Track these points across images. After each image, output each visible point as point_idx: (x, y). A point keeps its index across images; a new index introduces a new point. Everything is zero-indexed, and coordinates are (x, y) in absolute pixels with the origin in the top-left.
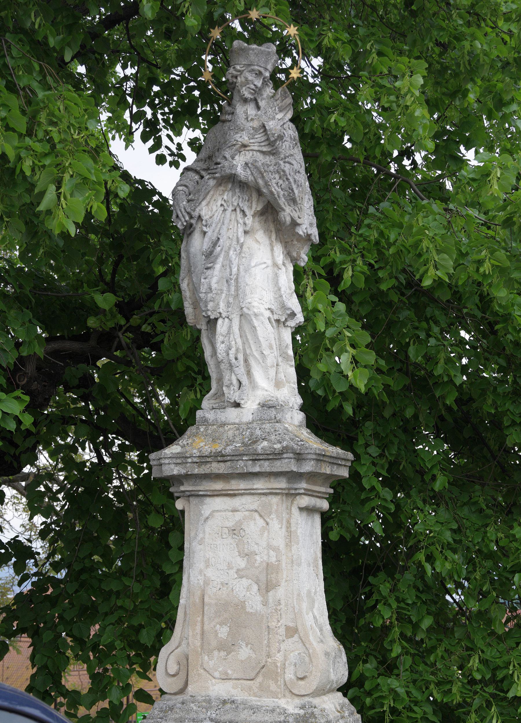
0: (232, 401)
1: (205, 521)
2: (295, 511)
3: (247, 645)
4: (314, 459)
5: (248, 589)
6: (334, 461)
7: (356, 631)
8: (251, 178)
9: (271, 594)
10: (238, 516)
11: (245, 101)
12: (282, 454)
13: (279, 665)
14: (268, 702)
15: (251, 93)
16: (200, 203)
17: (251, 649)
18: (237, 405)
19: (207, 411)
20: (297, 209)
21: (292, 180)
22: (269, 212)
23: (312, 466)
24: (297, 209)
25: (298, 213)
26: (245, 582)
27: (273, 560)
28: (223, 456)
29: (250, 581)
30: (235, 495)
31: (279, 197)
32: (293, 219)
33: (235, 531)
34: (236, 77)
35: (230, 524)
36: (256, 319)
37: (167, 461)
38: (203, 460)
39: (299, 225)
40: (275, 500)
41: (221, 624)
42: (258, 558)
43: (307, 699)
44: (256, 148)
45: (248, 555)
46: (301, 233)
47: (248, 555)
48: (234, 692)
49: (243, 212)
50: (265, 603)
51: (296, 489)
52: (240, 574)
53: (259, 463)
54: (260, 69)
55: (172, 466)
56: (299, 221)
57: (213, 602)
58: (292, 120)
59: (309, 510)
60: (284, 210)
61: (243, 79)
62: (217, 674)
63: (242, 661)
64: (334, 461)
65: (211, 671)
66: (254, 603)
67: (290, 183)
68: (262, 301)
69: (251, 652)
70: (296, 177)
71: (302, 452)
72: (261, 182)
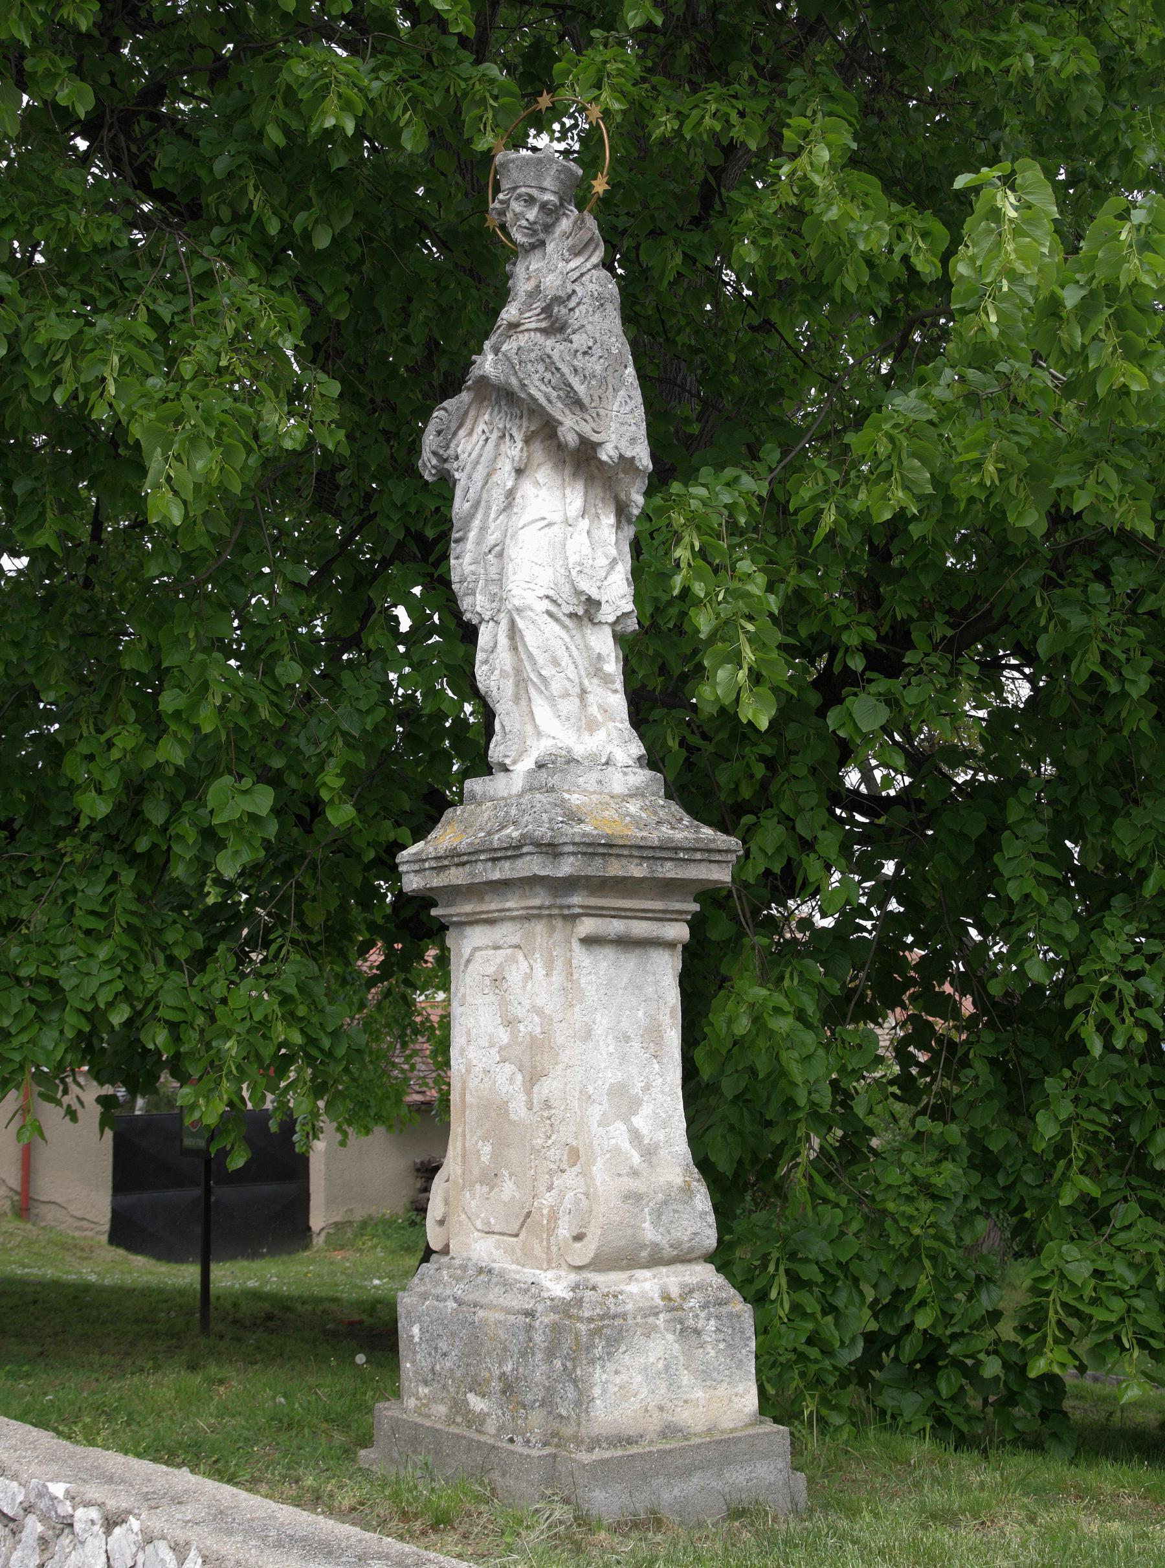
1: (466, 966)
2: (576, 945)
4: (573, 854)
5: (511, 1080)
6: (709, 853)
12: (521, 846)
13: (545, 1212)
14: (529, 1273)
15: (526, 235)
16: (455, 434)
20: (588, 418)
21: (565, 369)
23: (572, 865)
24: (588, 418)
25: (594, 425)
26: (508, 1068)
28: (459, 855)
31: (550, 402)
33: (498, 981)
35: (491, 970)
36: (522, 618)
39: (600, 444)
40: (539, 927)
41: (485, 1139)
42: (521, 1027)
43: (586, 1275)
44: (533, 325)
47: (510, 1022)
48: (497, 1254)
51: (569, 907)
54: (528, 190)
56: (595, 438)
57: (474, 1101)
60: (561, 423)
63: (505, 1204)
64: (709, 853)
67: (563, 375)
68: (532, 586)
70: (576, 363)
71: (556, 841)
72: (514, 381)
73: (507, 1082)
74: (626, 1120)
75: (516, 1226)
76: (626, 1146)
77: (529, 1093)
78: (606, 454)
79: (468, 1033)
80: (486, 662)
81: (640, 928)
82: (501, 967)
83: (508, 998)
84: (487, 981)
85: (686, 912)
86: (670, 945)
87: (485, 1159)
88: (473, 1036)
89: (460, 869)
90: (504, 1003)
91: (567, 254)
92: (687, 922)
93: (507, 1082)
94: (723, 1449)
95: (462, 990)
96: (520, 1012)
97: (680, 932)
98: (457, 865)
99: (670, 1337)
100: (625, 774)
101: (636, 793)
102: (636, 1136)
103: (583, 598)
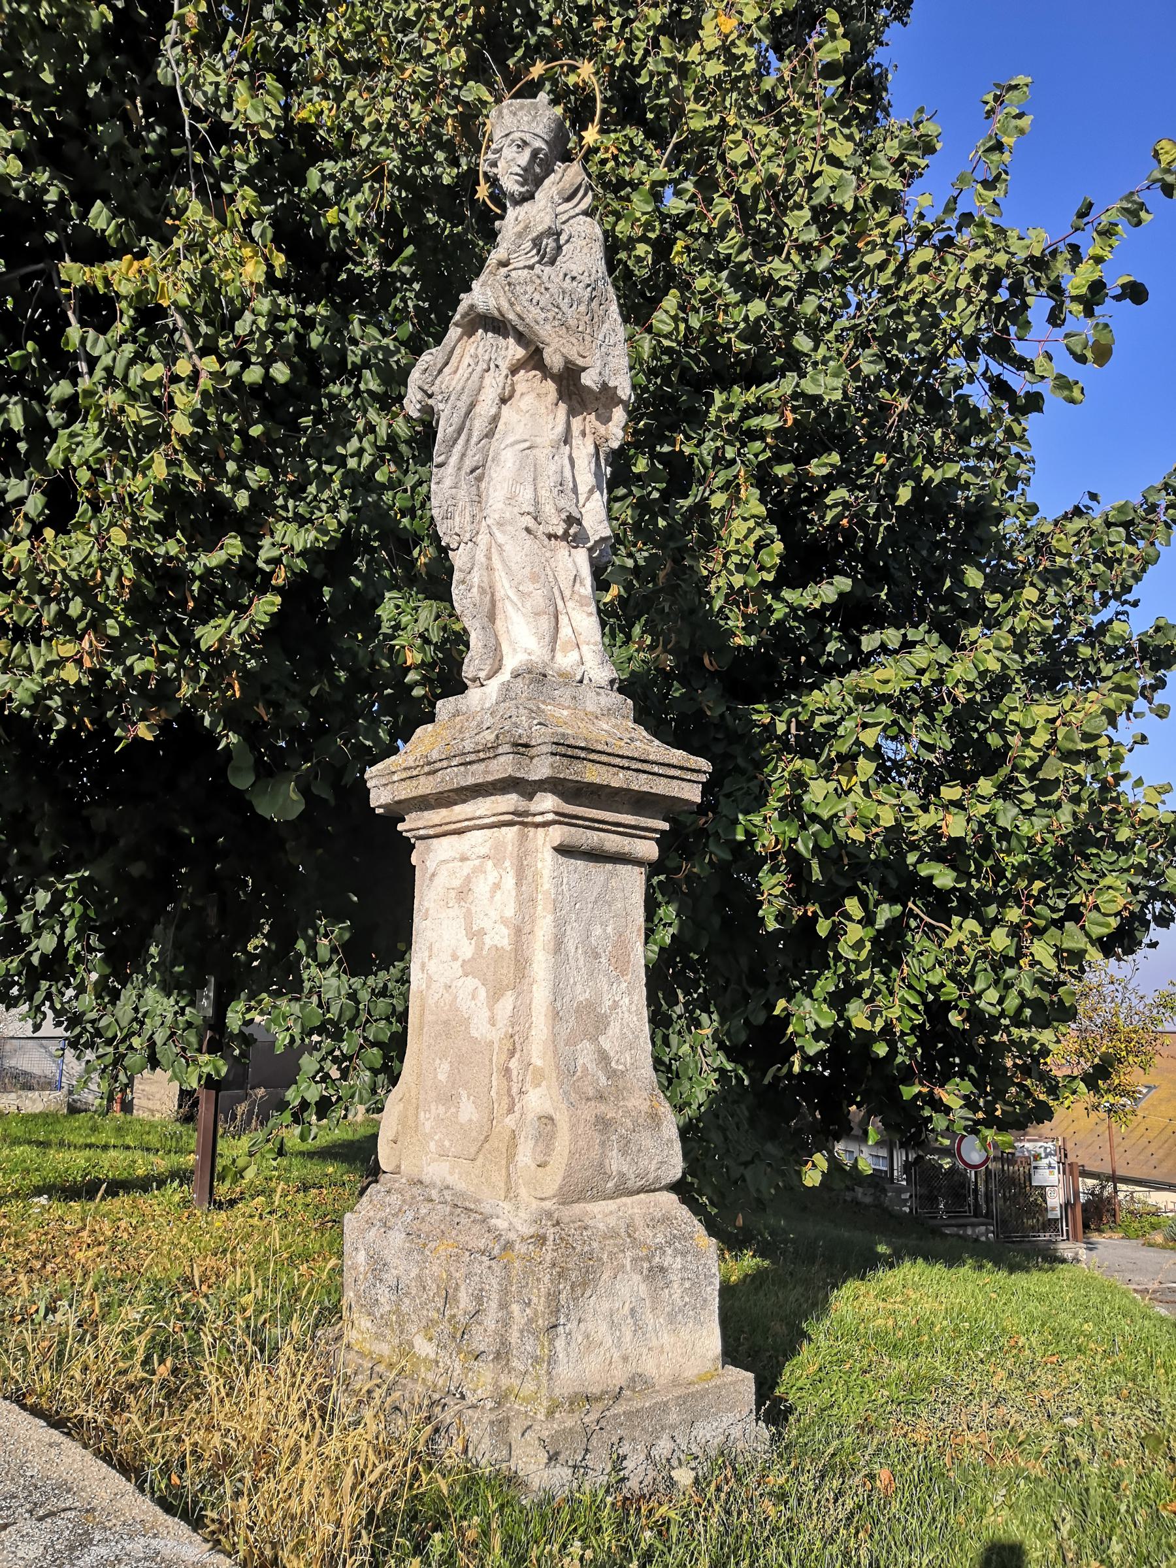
16: (440, 371)
35: (457, 883)
44: (521, 264)
56: (580, 362)
73: (471, 997)
74: (594, 1039)
75: (473, 1150)
76: (592, 1067)
77: (491, 1009)
78: (589, 379)
79: (430, 948)
80: (463, 582)
81: (613, 842)
82: (468, 879)
83: (473, 909)
84: (453, 894)
85: (655, 831)
86: (638, 862)
87: (442, 1077)
88: (435, 950)
89: (430, 778)
90: (468, 917)
91: (556, 198)
92: (657, 841)
93: (471, 997)
94: (694, 1402)
95: (426, 904)
96: (486, 924)
97: (649, 850)
98: (428, 774)
99: (637, 1278)
100: (598, 694)
101: (609, 712)
102: (603, 1058)
103: (564, 516)
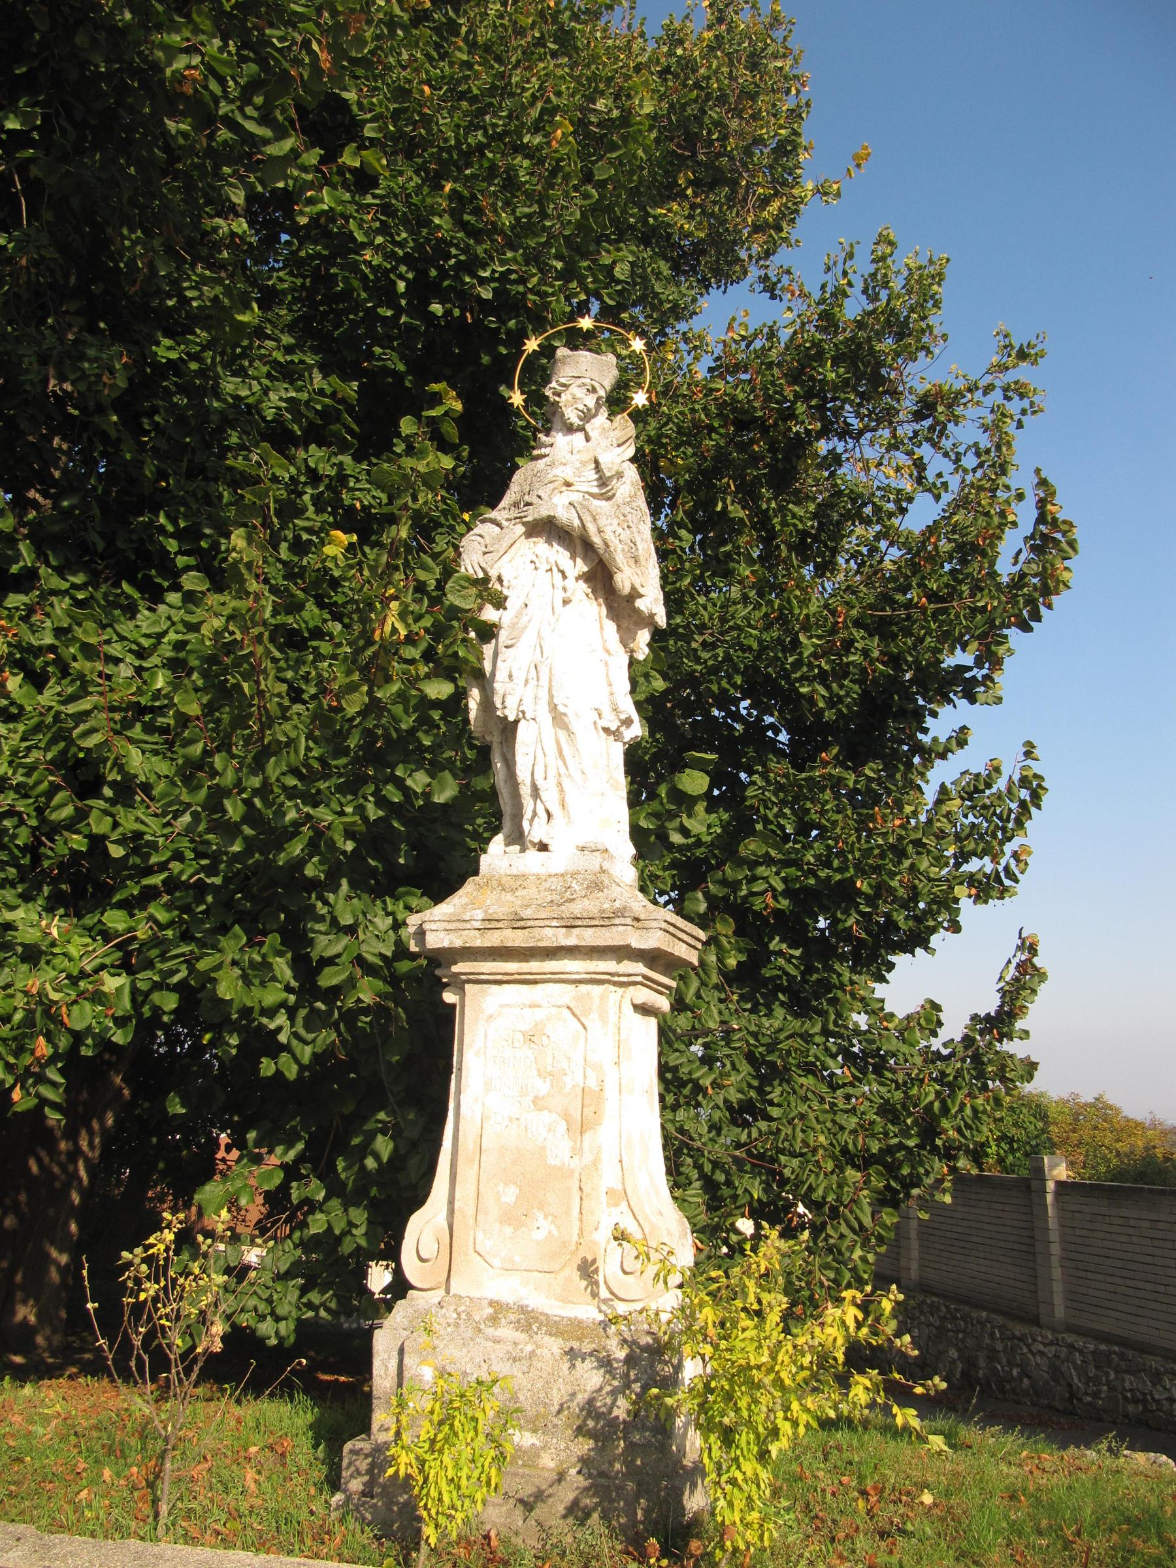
0: (536, 840)
3: (546, 1217)
7: (65, 503)
8: (577, 523)
9: (587, 1136)
10: (540, 1014)
11: (570, 429)
17: (552, 1222)
18: (543, 847)
19: (497, 856)
22: (600, 577)
27: (592, 1084)
29: (554, 1116)
30: (535, 982)
32: (633, 588)
34: (559, 395)
37: (433, 926)
38: (490, 923)
39: (641, 596)
42: (567, 1079)
45: (553, 1076)
46: (643, 608)
47: (553, 1076)
49: (563, 572)
50: (577, 1151)
52: (538, 1103)
53: (576, 931)
55: (442, 934)
56: (641, 591)
58: (633, 460)
59: (644, 1010)
61: (569, 397)
62: (496, 1262)
65: (487, 1257)
66: (560, 1149)
69: (553, 1227)
72: (591, 528)
